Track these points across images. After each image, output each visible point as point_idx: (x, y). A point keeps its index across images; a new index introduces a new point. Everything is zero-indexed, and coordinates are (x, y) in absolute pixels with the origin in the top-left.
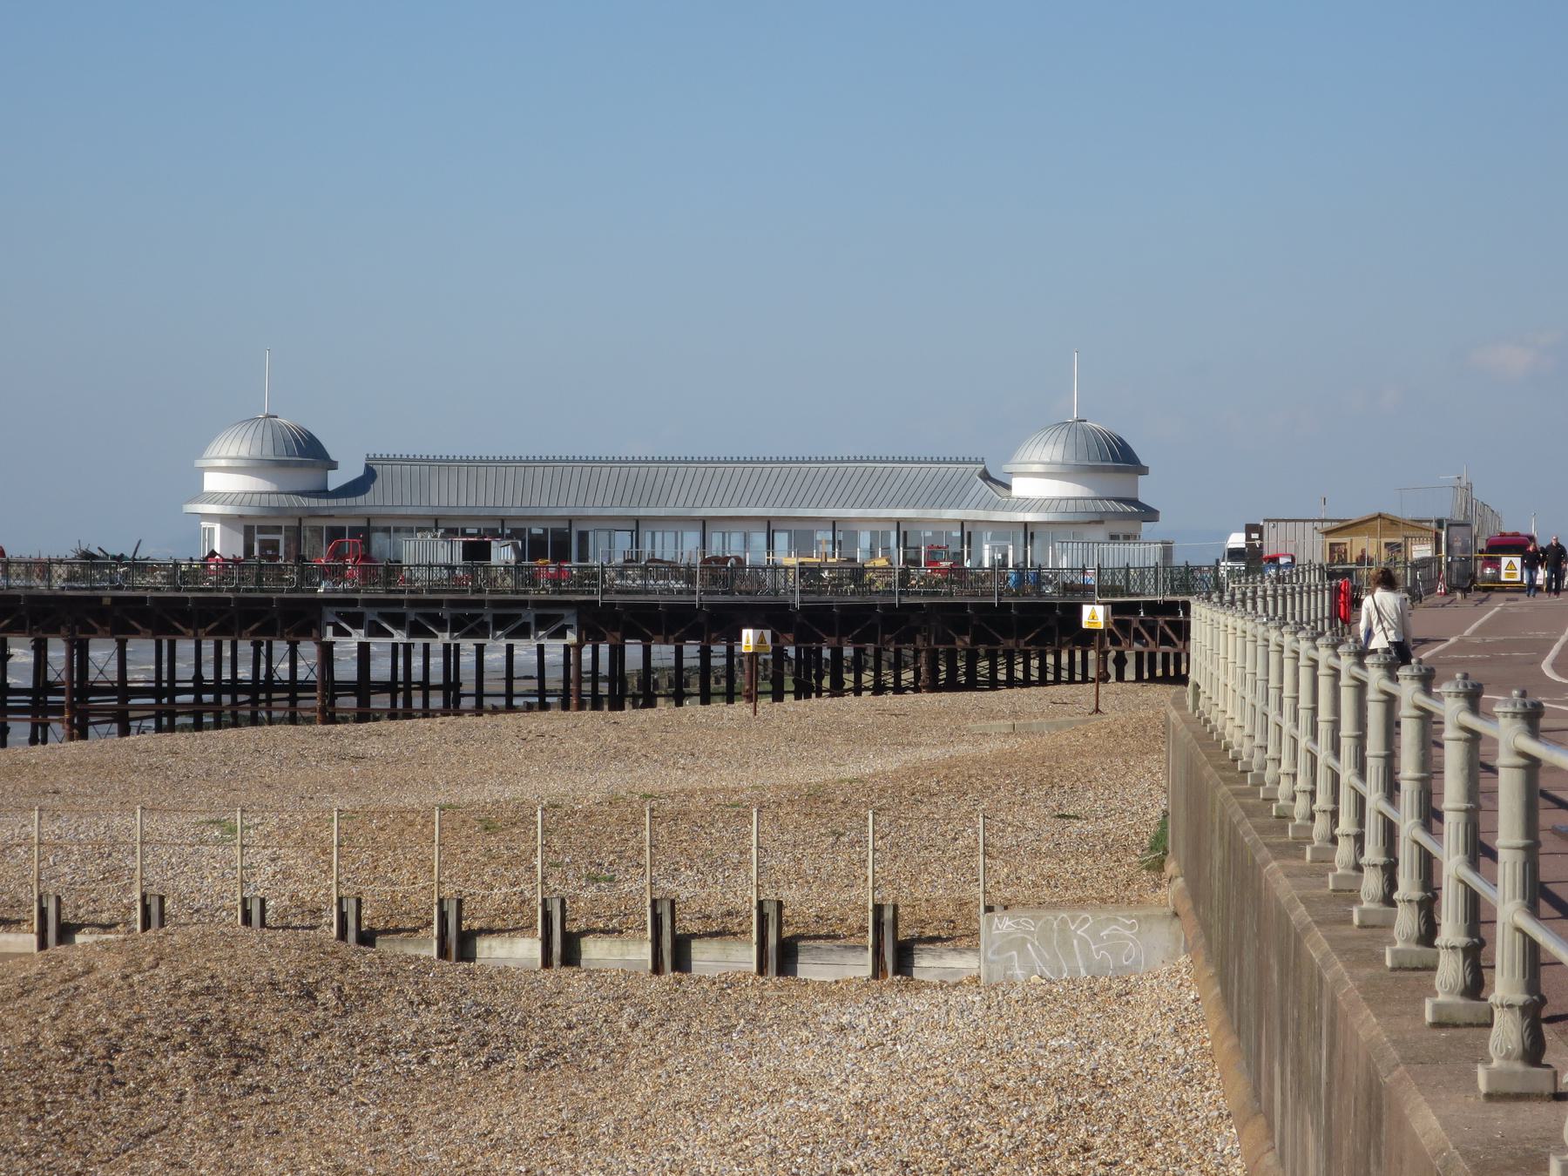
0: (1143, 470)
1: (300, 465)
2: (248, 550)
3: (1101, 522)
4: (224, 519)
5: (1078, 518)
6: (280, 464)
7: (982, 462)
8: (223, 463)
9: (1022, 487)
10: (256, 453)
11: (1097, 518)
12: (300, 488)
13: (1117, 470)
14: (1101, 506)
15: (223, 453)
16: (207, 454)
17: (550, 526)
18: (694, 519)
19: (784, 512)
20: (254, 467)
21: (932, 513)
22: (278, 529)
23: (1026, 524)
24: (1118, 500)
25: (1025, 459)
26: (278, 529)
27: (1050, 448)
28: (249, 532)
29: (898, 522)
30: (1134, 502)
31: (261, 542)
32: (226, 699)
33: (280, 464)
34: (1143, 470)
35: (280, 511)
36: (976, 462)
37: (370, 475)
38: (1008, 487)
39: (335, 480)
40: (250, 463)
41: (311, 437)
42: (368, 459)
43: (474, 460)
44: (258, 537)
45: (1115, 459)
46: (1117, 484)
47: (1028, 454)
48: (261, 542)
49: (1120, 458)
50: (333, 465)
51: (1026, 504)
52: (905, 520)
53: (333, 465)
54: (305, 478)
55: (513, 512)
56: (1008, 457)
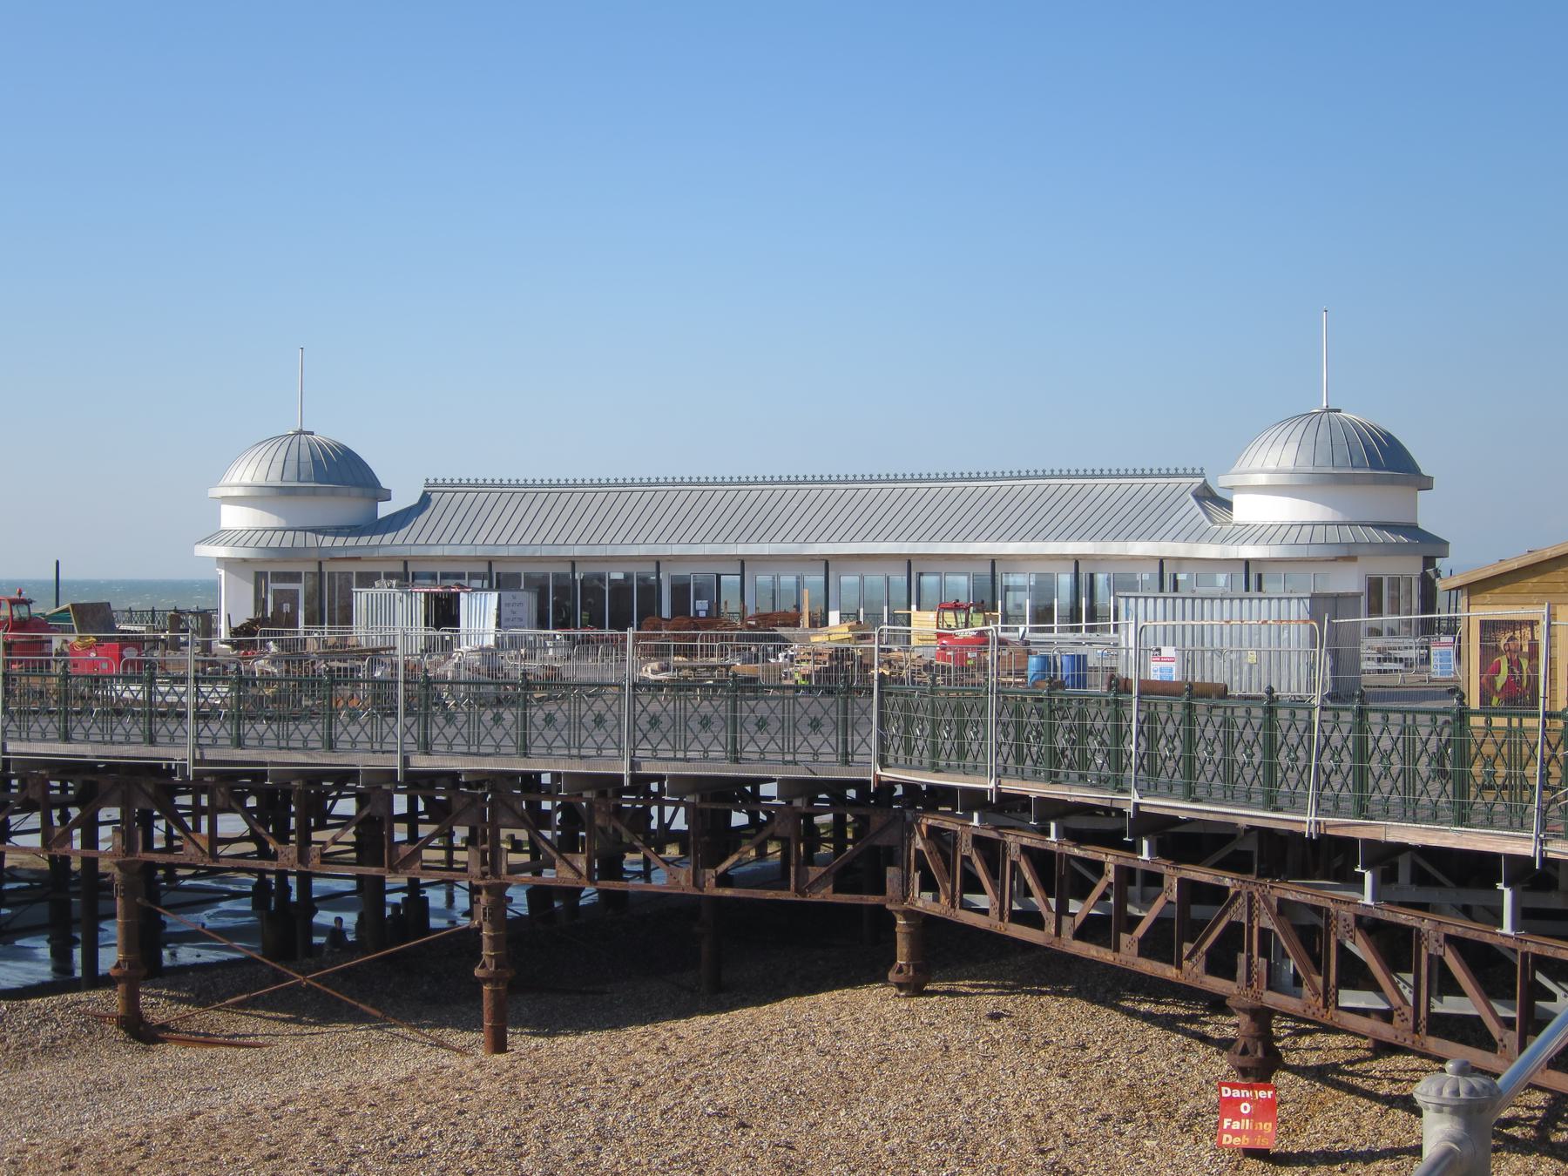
0: (1426, 483)
1: (313, 492)
2: (260, 603)
3: (1351, 558)
4: (227, 563)
5: (1313, 552)
6: (1339, 480)
7: (1201, 475)
8: (1262, 479)
9: (1247, 509)
10: (260, 479)
11: (1343, 552)
12: (318, 523)
13: (1376, 481)
14: (1348, 535)
15: (1257, 465)
16: (1244, 463)
17: (636, 569)
18: (812, 558)
19: (676, 550)
20: (260, 497)
21: (1114, 548)
22: (295, 577)
23: (1247, 562)
24: (317, 531)
25: (1244, 467)
26: (295, 577)
27: (1277, 449)
28: (260, 577)
29: (1077, 561)
30: (1411, 530)
31: (277, 593)
32: (107, 738)
33: (284, 492)
34: (1426, 483)
35: (283, 553)
36: (1194, 475)
37: (425, 500)
38: (1228, 505)
39: (384, 510)
40: (256, 492)
41: (1389, 438)
42: (427, 485)
43: (460, 485)
44: (273, 586)
45: (1375, 465)
46: (1384, 502)
47: (1260, 458)
48: (277, 593)
49: (1386, 460)
50: (386, 495)
51: (1249, 533)
52: (1085, 557)
53: (386, 495)
54: (343, 508)
55: (503, 552)
56: (1229, 462)
